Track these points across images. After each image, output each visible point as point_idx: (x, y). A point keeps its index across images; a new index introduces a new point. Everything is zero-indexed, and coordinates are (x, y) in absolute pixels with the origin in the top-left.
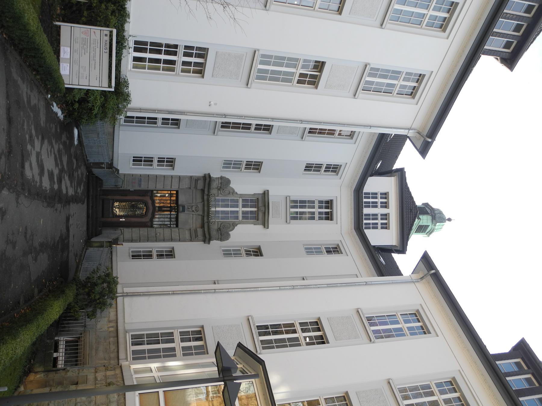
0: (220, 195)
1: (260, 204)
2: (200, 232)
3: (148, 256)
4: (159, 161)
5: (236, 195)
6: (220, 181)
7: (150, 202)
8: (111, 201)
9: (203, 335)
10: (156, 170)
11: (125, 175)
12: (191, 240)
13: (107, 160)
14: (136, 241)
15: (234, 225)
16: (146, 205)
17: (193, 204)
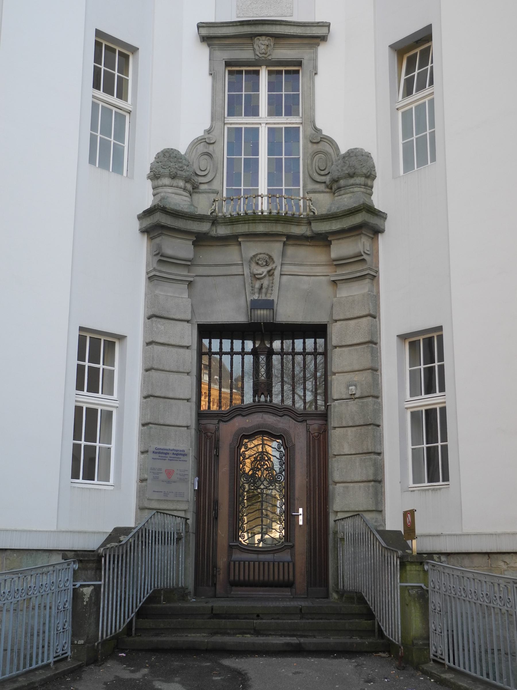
0: (215, 186)
1: (246, 54)
2: (341, 249)
3: (432, 425)
4: (93, 388)
5: (216, 133)
6: (166, 181)
7: (239, 423)
8: (237, 556)
9: (423, 409)
10: (125, 398)
11: (141, 508)
12: (373, 277)
13: (65, 578)
14: (379, 468)
15: (318, 139)
16: (251, 437)
17: (247, 272)
